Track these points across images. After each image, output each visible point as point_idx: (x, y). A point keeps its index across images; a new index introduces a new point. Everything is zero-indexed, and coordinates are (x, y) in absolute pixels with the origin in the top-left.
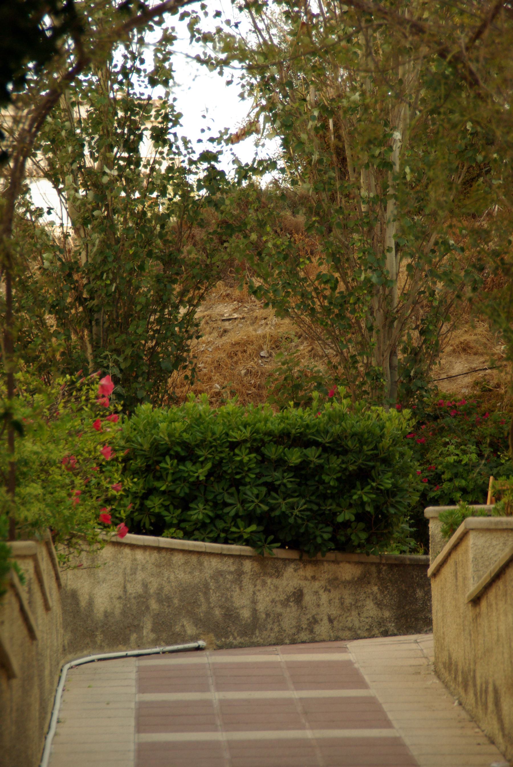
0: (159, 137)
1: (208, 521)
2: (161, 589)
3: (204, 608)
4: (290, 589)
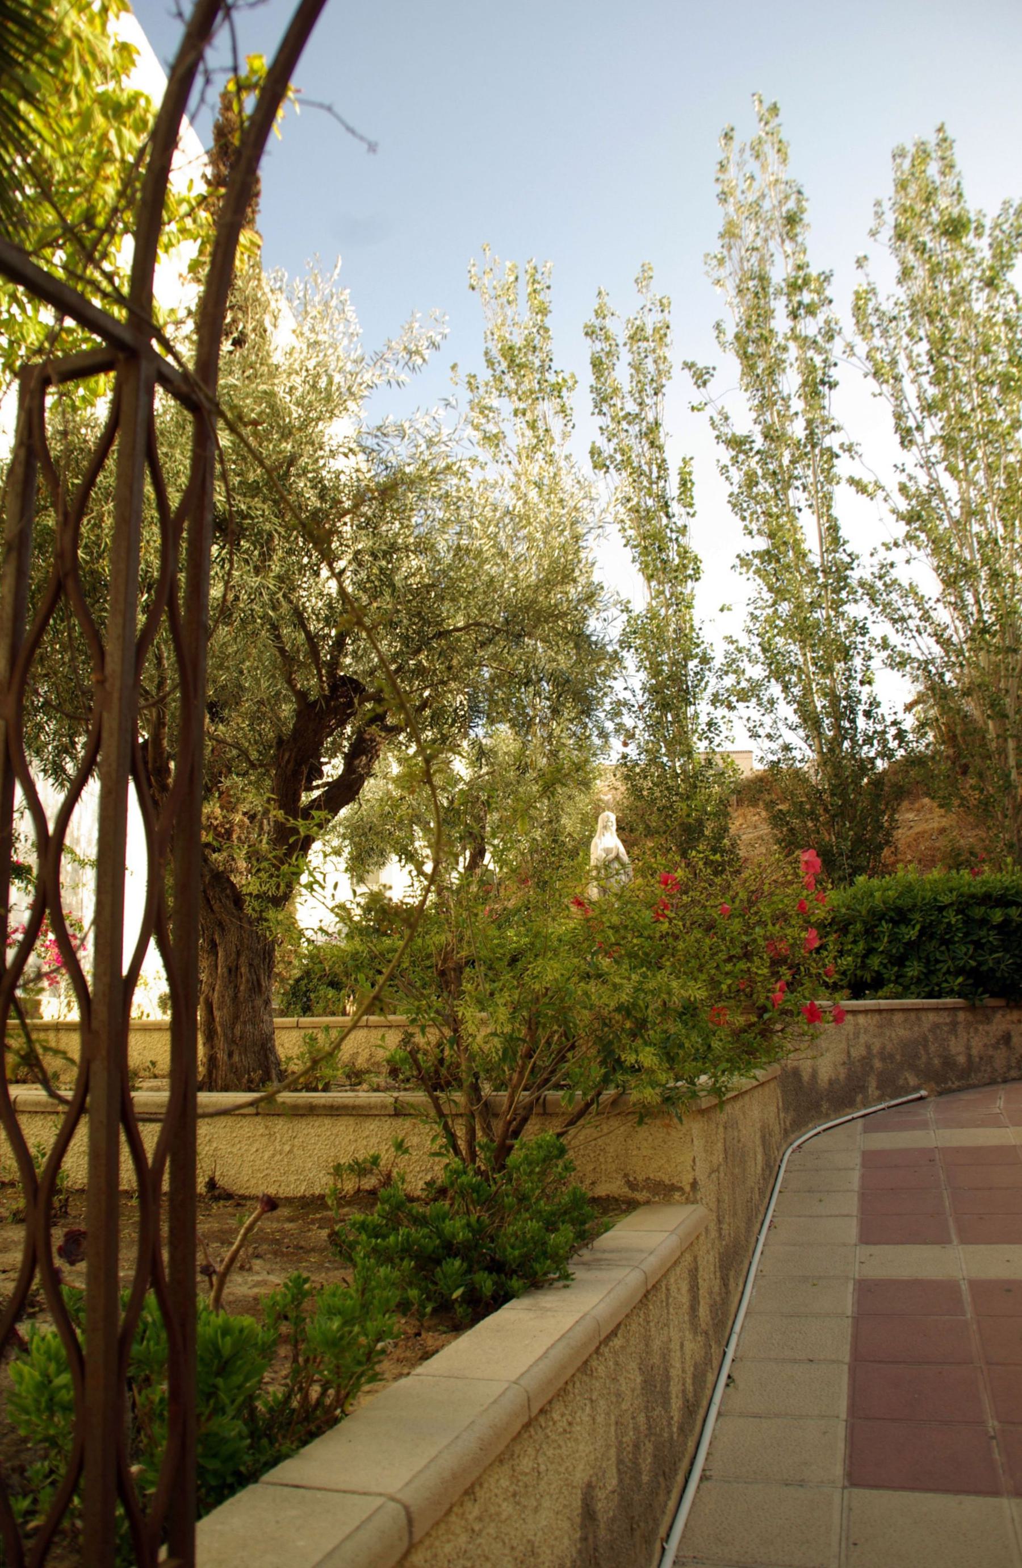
0: (868, 714)
1: (922, 977)
2: (883, 1048)
3: (924, 1059)
4: (999, 1033)
